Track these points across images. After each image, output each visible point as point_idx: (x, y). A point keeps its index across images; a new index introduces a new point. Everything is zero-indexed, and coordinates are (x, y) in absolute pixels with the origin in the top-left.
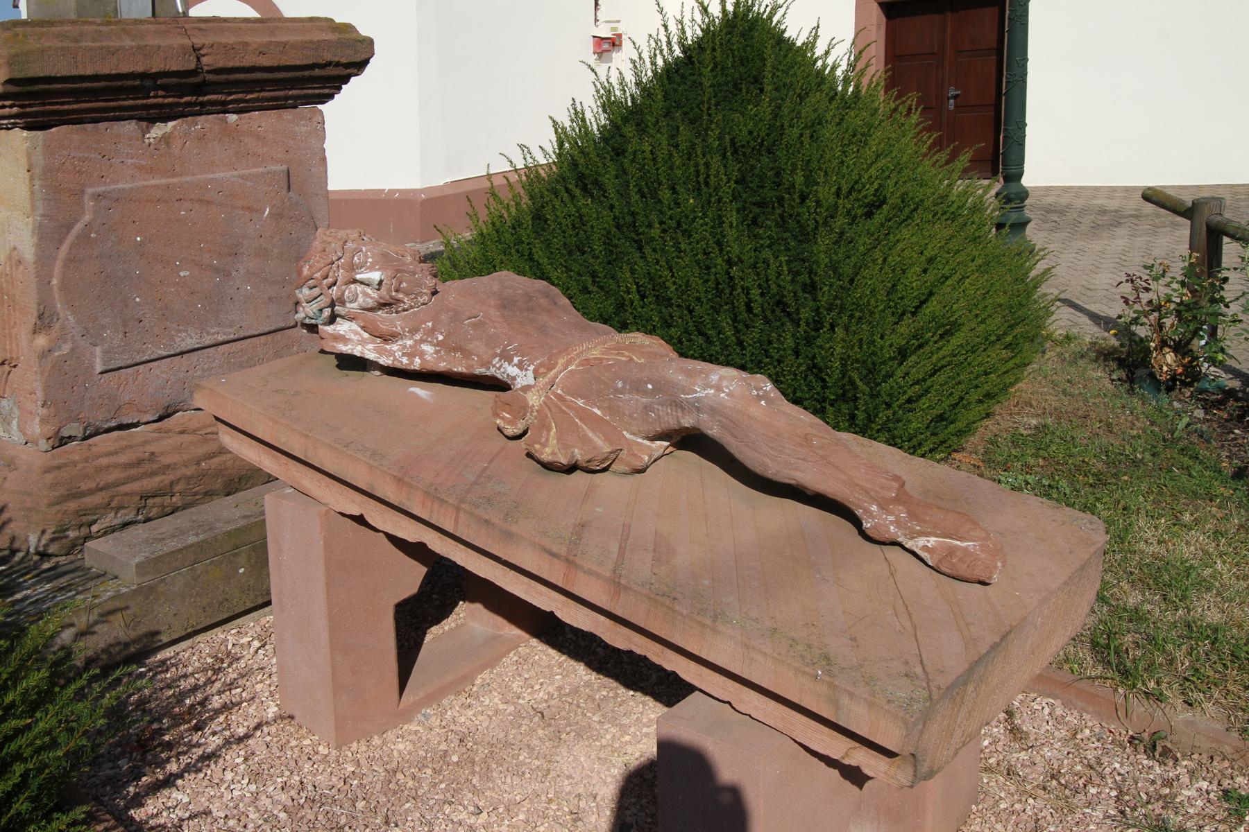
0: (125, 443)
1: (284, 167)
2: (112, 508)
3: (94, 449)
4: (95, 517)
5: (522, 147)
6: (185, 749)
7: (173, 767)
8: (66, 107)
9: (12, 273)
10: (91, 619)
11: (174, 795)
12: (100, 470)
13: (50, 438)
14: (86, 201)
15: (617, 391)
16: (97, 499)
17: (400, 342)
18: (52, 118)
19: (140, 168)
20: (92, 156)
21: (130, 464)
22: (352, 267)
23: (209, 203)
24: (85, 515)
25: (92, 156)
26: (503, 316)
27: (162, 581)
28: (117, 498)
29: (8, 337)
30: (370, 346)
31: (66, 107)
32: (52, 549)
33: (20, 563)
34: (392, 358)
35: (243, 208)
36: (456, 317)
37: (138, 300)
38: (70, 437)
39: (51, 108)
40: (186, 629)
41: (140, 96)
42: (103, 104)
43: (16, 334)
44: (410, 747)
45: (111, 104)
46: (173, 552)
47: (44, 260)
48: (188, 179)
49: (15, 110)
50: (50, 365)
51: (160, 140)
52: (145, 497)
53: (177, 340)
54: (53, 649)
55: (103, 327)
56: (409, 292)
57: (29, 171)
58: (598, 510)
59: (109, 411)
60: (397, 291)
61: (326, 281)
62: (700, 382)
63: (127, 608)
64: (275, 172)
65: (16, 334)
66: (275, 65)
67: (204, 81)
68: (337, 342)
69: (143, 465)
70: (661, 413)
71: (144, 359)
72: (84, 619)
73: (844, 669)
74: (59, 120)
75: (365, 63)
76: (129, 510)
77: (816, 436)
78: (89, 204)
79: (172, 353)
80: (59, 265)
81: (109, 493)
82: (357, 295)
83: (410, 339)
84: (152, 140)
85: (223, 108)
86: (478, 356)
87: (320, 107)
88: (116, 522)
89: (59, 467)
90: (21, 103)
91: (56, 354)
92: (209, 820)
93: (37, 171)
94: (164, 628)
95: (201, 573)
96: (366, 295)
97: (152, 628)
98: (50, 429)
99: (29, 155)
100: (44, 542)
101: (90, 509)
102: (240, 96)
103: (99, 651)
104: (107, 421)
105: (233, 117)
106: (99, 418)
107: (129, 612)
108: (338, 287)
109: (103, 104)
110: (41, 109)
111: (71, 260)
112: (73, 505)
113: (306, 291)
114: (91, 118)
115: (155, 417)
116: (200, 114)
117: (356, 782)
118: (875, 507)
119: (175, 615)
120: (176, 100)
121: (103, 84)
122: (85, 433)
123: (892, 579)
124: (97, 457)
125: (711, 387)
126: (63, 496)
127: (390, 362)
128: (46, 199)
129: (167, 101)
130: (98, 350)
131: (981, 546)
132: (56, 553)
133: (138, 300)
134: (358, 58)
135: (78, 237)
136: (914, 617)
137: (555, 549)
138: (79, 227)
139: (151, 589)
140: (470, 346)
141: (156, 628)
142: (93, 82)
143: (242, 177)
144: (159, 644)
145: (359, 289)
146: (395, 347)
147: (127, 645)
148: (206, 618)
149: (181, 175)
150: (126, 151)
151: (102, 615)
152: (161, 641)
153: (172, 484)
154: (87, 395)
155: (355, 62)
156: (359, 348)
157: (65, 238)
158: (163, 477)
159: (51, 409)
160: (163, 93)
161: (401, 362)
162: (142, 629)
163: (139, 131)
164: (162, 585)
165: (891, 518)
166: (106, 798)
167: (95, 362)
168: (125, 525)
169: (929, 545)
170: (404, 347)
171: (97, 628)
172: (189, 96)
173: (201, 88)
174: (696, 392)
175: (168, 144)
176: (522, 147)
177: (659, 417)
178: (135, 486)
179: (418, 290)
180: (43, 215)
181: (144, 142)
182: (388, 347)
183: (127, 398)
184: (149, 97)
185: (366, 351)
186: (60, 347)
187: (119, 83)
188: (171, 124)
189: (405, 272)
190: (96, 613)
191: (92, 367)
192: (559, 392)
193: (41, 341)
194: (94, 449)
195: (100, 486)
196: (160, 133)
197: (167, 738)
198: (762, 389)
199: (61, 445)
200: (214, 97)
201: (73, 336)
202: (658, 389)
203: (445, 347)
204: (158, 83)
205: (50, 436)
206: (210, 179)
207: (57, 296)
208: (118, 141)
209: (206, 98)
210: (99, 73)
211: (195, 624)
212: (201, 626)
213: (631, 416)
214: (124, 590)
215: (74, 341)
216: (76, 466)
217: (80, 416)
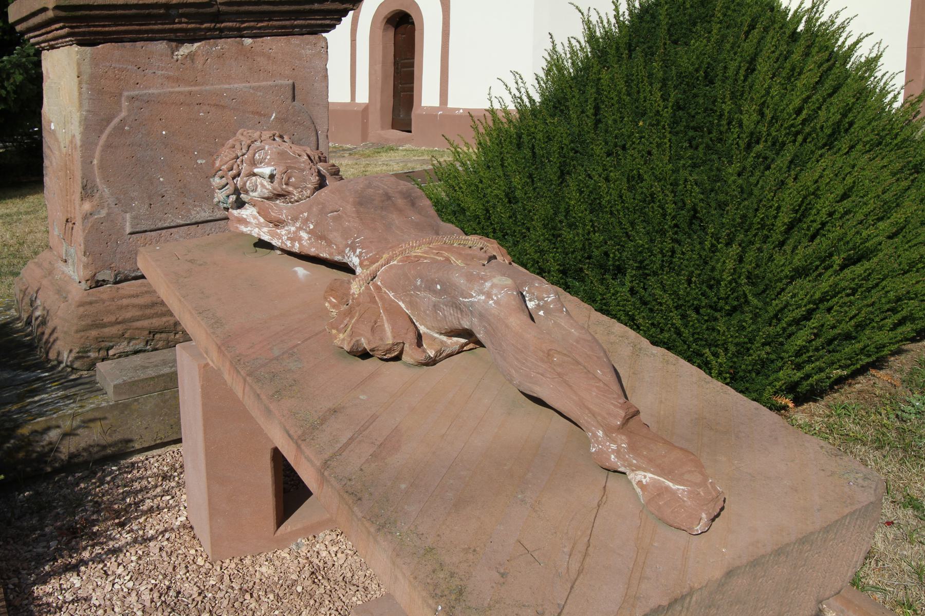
1: (291, 82)
2: (125, 338)
3: (121, 291)
4: (111, 344)
5: (515, 73)
6: (105, 540)
7: (86, 555)
8: (107, 29)
10: (75, 424)
11: (72, 579)
12: (121, 308)
13: (88, 280)
15: (417, 288)
16: (114, 330)
17: (286, 228)
19: (168, 78)
20: (129, 67)
21: (145, 306)
22: (254, 163)
23: (223, 107)
25: (129, 67)
26: (358, 212)
27: (136, 400)
28: (129, 331)
30: (265, 229)
31: (107, 29)
32: (77, 365)
33: (60, 372)
35: (253, 113)
36: (323, 212)
37: (161, 179)
38: (104, 281)
40: (155, 440)
42: (137, 28)
44: (271, 572)
45: (144, 27)
46: (146, 379)
47: (88, 145)
48: (208, 88)
49: (66, 30)
50: (90, 225)
51: (187, 56)
52: (153, 332)
53: (193, 213)
54: (42, 444)
55: (132, 199)
58: (362, 397)
60: (287, 184)
62: (476, 288)
63: (105, 418)
67: (219, 10)
69: (155, 308)
70: (446, 313)
71: (165, 225)
72: (69, 423)
73: (469, 608)
74: (103, 39)
76: (139, 341)
77: (559, 353)
78: (125, 104)
79: (189, 222)
81: (125, 327)
82: (257, 186)
83: (293, 226)
84: (179, 57)
85: (240, 34)
86: (336, 245)
87: (324, 35)
88: (128, 349)
89: (91, 303)
90: (70, 24)
92: (86, 606)
93: (85, 77)
94: (135, 438)
96: (263, 186)
97: (126, 437)
98: (89, 273)
99: (79, 65)
100: (70, 359)
101: (107, 338)
102: (252, 24)
103: (81, 449)
104: (134, 271)
105: (248, 41)
107: (107, 422)
109: (137, 28)
110: (87, 29)
111: (108, 146)
112: (94, 333)
114: (129, 38)
116: (221, 38)
117: (210, 595)
118: (601, 432)
119: (146, 428)
120: (198, 26)
121: (134, 11)
122: (116, 278)
123: (595, 511)
124: (122, 298)
125: (483, 293)
129: (190, 26)
130: (128, 216)
131: (689, 492)
132: (80, 368)
133: (161, 179)
135: (115, 129)
136: (588, 560)
137: (291, 432)
138: (116, 121)
139: (126, 406)
140: (331, 236)
141: (130, 437)
142: (125, 10)
143: (253, 88)
144: (132, 449)
145: (259, 180)
146: (284, 232)
147: (104, 447)
148: (173, 433)
149: (202, 85)
150: (157, 64)
151: (84, 422)
152: (133, 447)
154: (119, 250)
156: (257, 230)
157: (105, 129)
159: (90, 258)
160: (186, 20)
161: (286, 245)
162: (117, 437)
163: (169, 50)
164: (135, 403)
165: (614, 447)
166: (24, 572)
167: (125, 225)
168: (136, 352)
169: (644, 481)
170: (289, 233)
171: (79, 431)
172: (207, 22)
174: (472, 296)
175: (193, 61)
176: (515, 73)
177: (445, 316)
178: (145, 323)
179: (304, 184)
180: (88, 111)
181: (172, 58)
182: (279, 231)
184: (174, 23)
185: (262, 233)
186: (99, 211)
187: (147, 11)
188: (196, 45)
189: (295, 168)
190: (79, 420)
191: (123, 228)
192: (379, 283)
193: (87, 206)
194: (121, 291)
197: (95, 529)
198: (543, 300)
199: (97, 286)
200: (230, 24)
201: (108, 204)
202: (444, 291)
203: (318, 235)
205: (87, 278)
207: (96, 172)
208: (150, 56)
210: (129, 3)
211: (163, 437)
212: (169, 440)
213: (425, 312)
214: (104, 404)
215: (109, 208)
217: (112, 266)
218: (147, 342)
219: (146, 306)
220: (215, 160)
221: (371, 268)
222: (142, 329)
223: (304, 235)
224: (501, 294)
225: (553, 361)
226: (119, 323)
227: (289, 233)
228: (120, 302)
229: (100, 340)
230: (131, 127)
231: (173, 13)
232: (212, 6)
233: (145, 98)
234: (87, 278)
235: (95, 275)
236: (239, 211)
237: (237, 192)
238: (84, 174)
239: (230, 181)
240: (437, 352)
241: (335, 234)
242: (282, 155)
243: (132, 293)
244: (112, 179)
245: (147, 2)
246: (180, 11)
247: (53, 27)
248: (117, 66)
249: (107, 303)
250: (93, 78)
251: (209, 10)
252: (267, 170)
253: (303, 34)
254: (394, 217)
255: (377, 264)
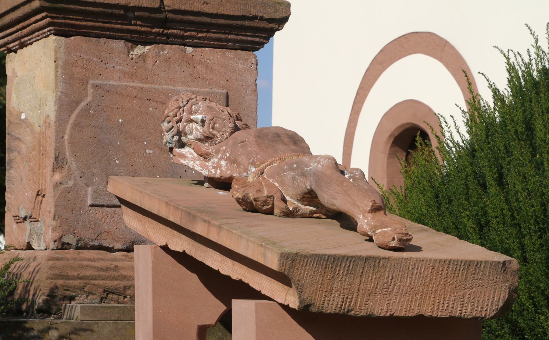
0: (101, 256)
1: (225, 91)
2: (85, 292)
8: (78, 23)
9: (45, 132)
12: (82, 267)
13: (55, 241)
14: (89, 88)
16: (77, 283)
18: (71, 29)
19: (124, 73)
20: (95, 59)
21: (101, 269)
22: (191, 113)
24: (67, 290)
25: (95, 59)
26: (257, 142)
28: (88, 286)
29: (41, 175)
30: (198, 162)
31: (78, 23)
34: (208, 171)
37: (117, 162)
38: (68, 244)
39: (69, 21)
41: (125, 22)
42: (102, 25)
43: (45, 173)
45: (107, 25)
47: (61, 122)
48: (156, 86)
50: (59, 192)
51: (140, 56)
55: (94, 175)
56: (219, 130)
57: (55, 62)
59: (94, 234)
60: (213, 128)
61: (175, 118)
64: (217, 93)
65: (45, 173)
66: (215, 12)
68: (181, 158)
69: (109, 272)
74: (75, 32)
75: (284, 20)
78: (90, 90)
80: (69, 126)
84: (134, 56)
85: (183, 42)
86: (243, 165)
91: (64, 186)
93: (60, 63)
95: (122, 328)
96: (197, 129)
98: (56, 236)
99: (56, 51)
101: (71, 287)
102: (193, 33)
104: (92, 240)
105: (190, 50)
106: (88, 236)
108: (182, 123)
109: (102, 25)
110: (63, 21)
111: (76, 125)
113: (166, 124)
114: (95, 34)
115: (124, 247)
116: (167, 44)
120: (149, 29)
121: (100, 9)
122: (78, 244)
124: (83, 260)
126: (56, 275)
127: (207, 173)
128: (64, 82)
130: (90, 189)
133: (117, 162)
134: (278, 15)
138: (83, 104)
145: (194, 126)
150: (116, 60)
153: (125, 288)
154: (81, 219)
155: (275, 19)
156: (192, 163)
157: (74, 110)
158: (120, 282)
159: (58, 221)
161: (211, 172)
163: (126, 48)
164: (96, 326)
172: (157, 28)
173: (165, 23)
174: (311, 166)
175: (144, 61)
179: (224, 129)
180: (62, 92)
181: (128, 56)
182: (207, 163)
183: (106, 228)
184: (131, 24)
185: (195, 165)
186: (67, 182)
187: (110, 11)
188: (148, 47)
189: (219, 118)
191: (85, 199)
193: (57, 177)
195: (80, 276)
196: (140, 52)
198: (353, 173)
204: (136, 15)
206: (170, 89)
209: (170, 31)
215: (75, 180)
216: (68, 261)
217: (75, 232)
218: (102, 299)
219: (101, 269)
220: (165, 109)
221: (261, 167)
222: (98, 286)
223: (223, 163)
224: (325, 161)
225: (343, 185)
226: (81, 278)
227: (213, 164)
228: (81, 263)
229: (66, 288)
230: (94, 110)
231: (130, 16)
232: (162, 12)
233: (106, 88)
234: (56, 238)
235: (62, 237)
236: (180, 149)
237: (179, 133)
238: (57, 146)
239: (175, 125)
240: (293, 208)
241: (243, 157)
242: (210, 108)
243: (90, 257)
244: (78, 154)
245: (110, 2)
246: (136, 14)
247: (33, 19)
248: (85, 57)
249: (70, 262)
250: (67, 65)
251: (158, 16)
252: (199, 117)
253: (236, 49)
254: (281, 147)
255: (264, 164)
